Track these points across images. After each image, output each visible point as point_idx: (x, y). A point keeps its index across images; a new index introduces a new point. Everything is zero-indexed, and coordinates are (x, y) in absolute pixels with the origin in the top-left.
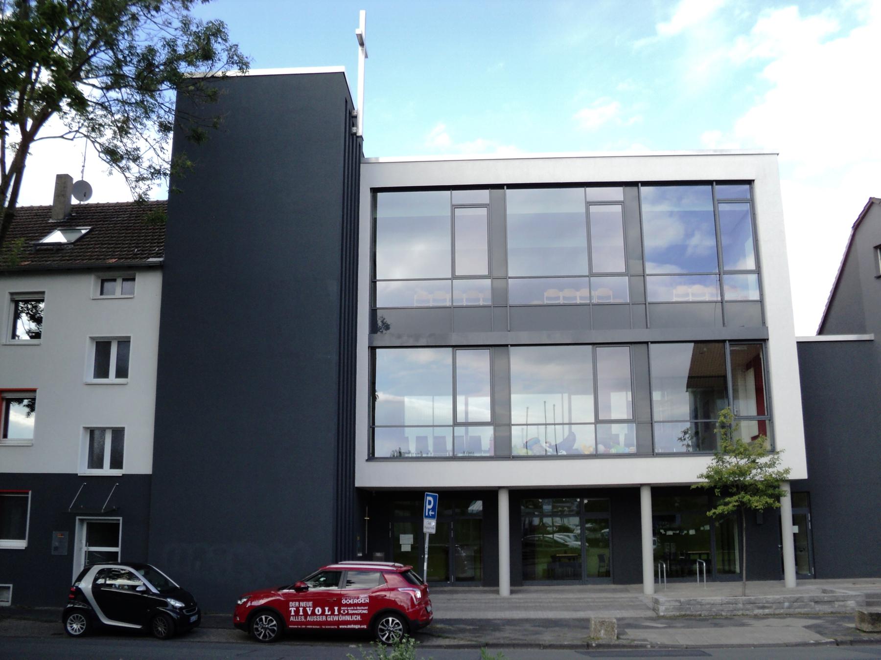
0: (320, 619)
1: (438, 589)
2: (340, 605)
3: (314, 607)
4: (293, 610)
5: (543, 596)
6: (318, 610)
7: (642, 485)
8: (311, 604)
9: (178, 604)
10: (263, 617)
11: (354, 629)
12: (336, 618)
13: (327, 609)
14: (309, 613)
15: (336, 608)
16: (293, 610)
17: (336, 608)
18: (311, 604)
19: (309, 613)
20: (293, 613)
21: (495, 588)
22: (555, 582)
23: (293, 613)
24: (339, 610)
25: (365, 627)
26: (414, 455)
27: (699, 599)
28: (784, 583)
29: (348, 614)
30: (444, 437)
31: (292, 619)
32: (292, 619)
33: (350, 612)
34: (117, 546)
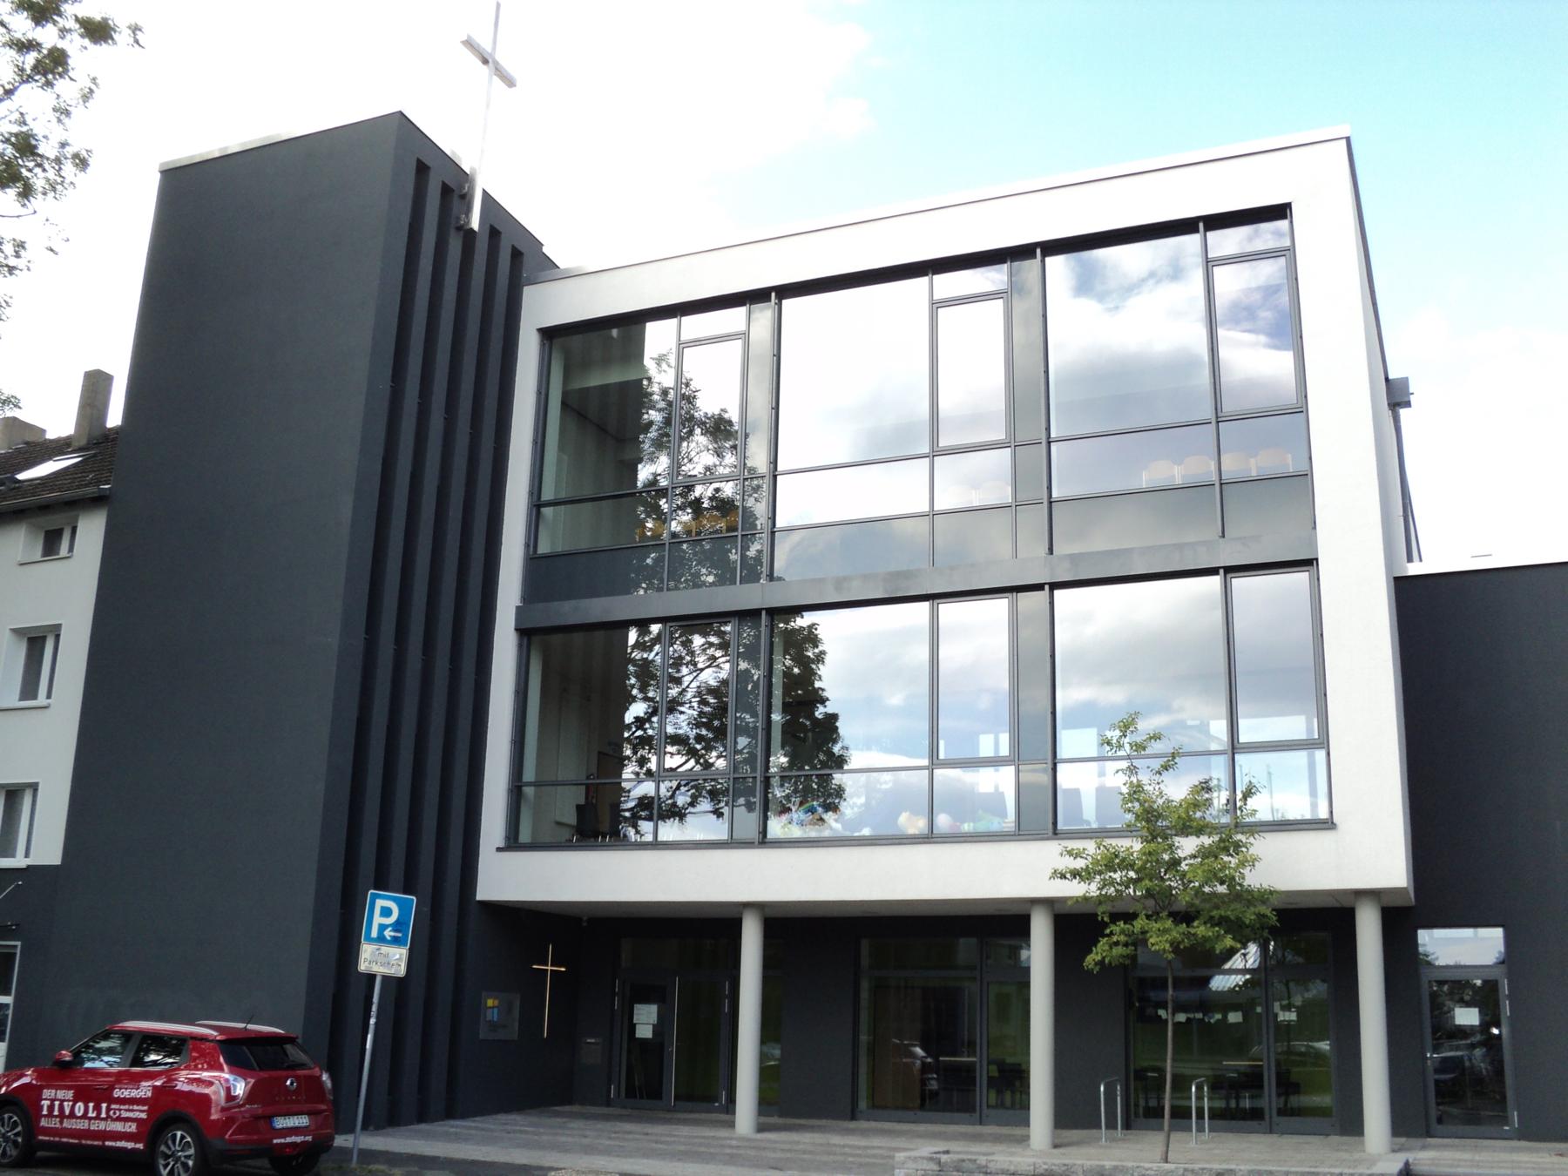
0: (82, 1125)
1: (697, 1116)
2: (112, 1101)
3: (75, 1102)
4: (46, 1103)
5: (836, 1139)
6: (80, 1108)
7: (1360, 894)
8: (70, 1094)
9: (302, 1121)
10: (179, 1134)
11: (124, 1149)
12: (102, 1126)
13: (91, 1105)
14: (67, 1112)
15: (104, 1105)
16: (46, 1103)
17: (104, 1105)
18: (70, 1094)
19: (67, 1112)
20: (45, 1112)
21: (1018, 1131)
22: (948, 1115)
23: (45, 1112)
24: (108, 1109)
25: (140, 1146)
26: (1094, 826)
27: (982, 1160)
28: (1363, 1143)
29: (119, 1119)
30: (13, 856)
31: (44, 1123)
32: (44, 1123)
33: (125, 1114)
34: (7, 993)
